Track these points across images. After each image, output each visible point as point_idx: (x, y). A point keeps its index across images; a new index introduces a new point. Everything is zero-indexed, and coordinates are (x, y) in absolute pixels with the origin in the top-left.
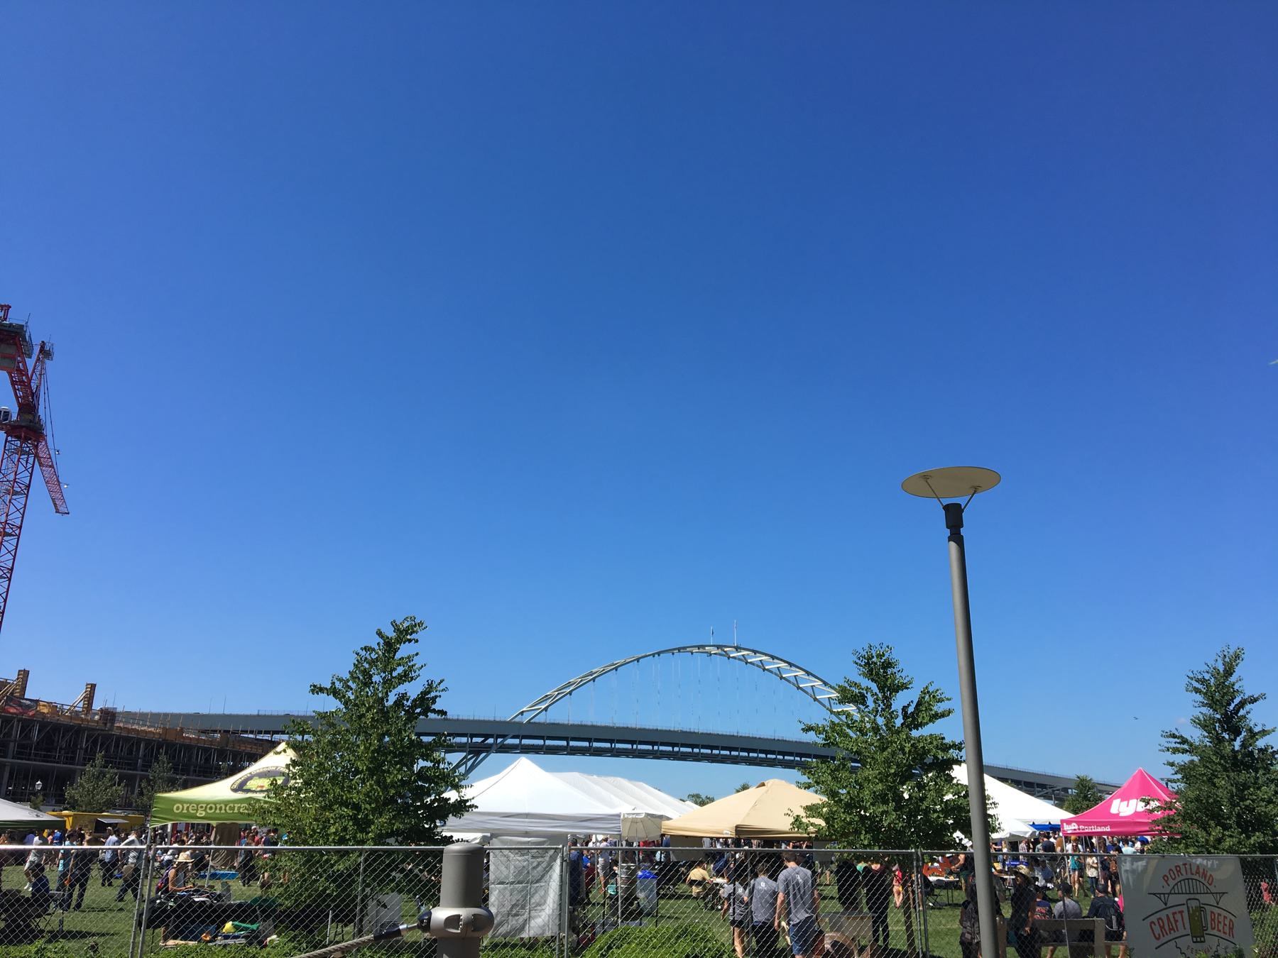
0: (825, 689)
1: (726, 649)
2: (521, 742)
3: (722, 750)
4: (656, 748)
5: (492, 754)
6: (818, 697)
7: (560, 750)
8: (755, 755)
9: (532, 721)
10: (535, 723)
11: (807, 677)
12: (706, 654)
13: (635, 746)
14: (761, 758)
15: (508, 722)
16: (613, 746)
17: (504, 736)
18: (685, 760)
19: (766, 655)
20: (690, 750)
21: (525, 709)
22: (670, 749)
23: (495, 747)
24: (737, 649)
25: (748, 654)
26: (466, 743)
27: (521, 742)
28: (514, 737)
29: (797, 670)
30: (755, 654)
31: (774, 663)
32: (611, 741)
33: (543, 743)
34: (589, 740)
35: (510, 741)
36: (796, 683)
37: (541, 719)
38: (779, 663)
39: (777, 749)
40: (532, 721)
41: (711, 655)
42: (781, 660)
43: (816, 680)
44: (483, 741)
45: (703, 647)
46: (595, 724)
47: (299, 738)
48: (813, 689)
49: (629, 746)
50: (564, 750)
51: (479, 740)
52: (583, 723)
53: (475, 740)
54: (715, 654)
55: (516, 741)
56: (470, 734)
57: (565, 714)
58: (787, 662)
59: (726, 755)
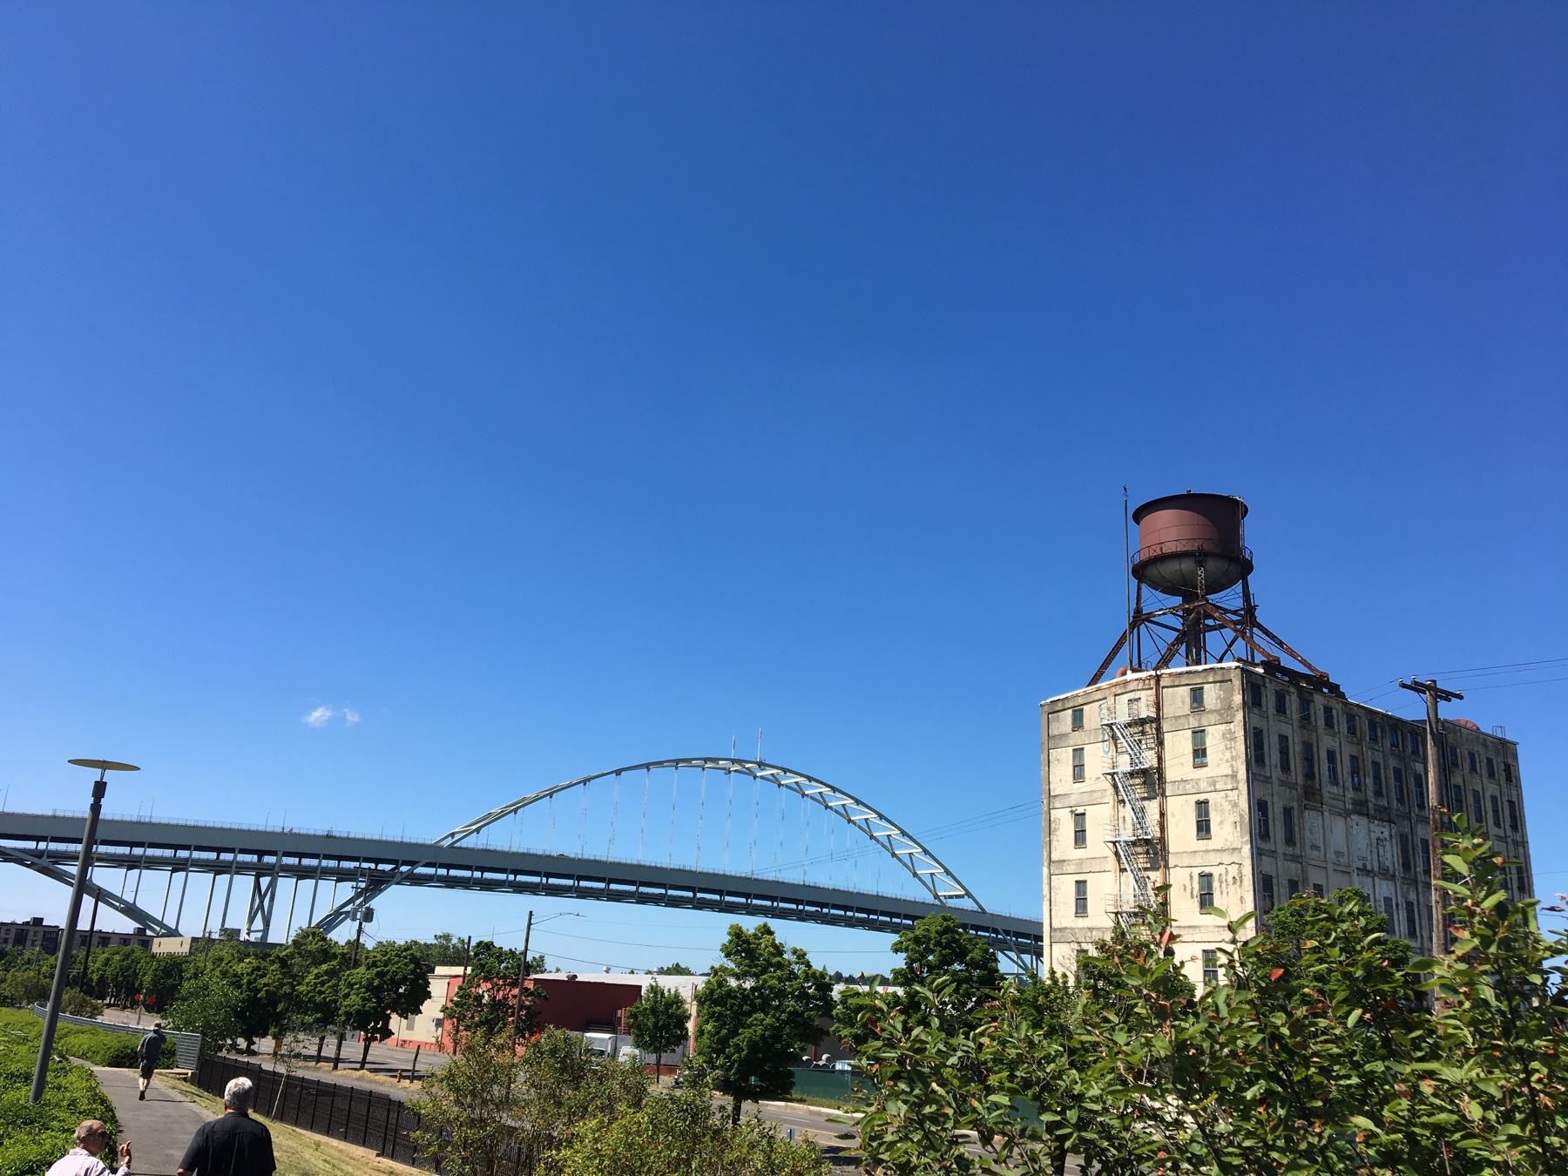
0: (902, 840)
1: (747, 766)
2: (638, 889)
3: (880, 915)
4: (801, 907)
5: (393, 886)
6: (875, 835)
7: (564, 890)
8: (898, 921)
9: (456, 845)
10: (460, 848)
11: (856, 807)
12: (723, 771)
13: (775, 904)
14: (882, 922)
15: (431, 846)
16: (749, 901)
17: (413, 864)
18: (833, 924)
19: (801, 775)
20: (794, 906)
21: (457, 830)
22: (794, 906)
23: (398, 877)
24: (761, 765)
25: (778, 774)
26: (505, 881)
27: (638, 889)
28: (428, 865)
29: (844, 797)
30: (785, 773)
31: (838, 799)
32: (747, 896)
33: (480, 876)
34: (720, 893)
35: (420, 870)
36: (866, 829)
37: (471, 842)
38: (794, 778)
39: (903, 912)
40: (456, 845)
41: (730, 772)
42: (822, 783)
43: (869, 811)
44: (393, 869)
45: (715, 760)
46: (598, 858)
47: (544, 880)
48: (889, 839)
49: (769, 903)
50: (632, 897)
51: (388, 867)
52: (531, 852)
53: (381, 867)
54: (735, 771)
55: (431, 871)
56: (578, 876)
57: (501, 838)
58: (921, 847)
59: (886, 922)
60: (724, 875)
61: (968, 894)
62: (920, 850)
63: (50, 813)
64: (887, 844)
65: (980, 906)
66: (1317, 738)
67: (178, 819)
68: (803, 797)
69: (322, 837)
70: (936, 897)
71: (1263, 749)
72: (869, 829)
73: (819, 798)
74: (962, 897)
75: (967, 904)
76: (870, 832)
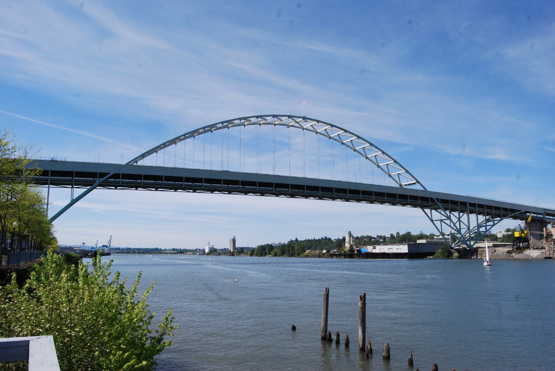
12: (286, 127)
37: (149, 162)
58: (405, 169)
60: (467, 196)
61: (418, 182)
62: (356, 137)
63: (466, 196)
64: (326, 134)
65: (424, 188)
66: (356, 261)
67: (45, 157)
68: (317, 134)
69: (49, 161)
70: (401, 185)
71: (361, 272)
72: (366, 154)
73: (338, 138)
74: (415, 183)
75: (418, 187)
76: (315, 130)
